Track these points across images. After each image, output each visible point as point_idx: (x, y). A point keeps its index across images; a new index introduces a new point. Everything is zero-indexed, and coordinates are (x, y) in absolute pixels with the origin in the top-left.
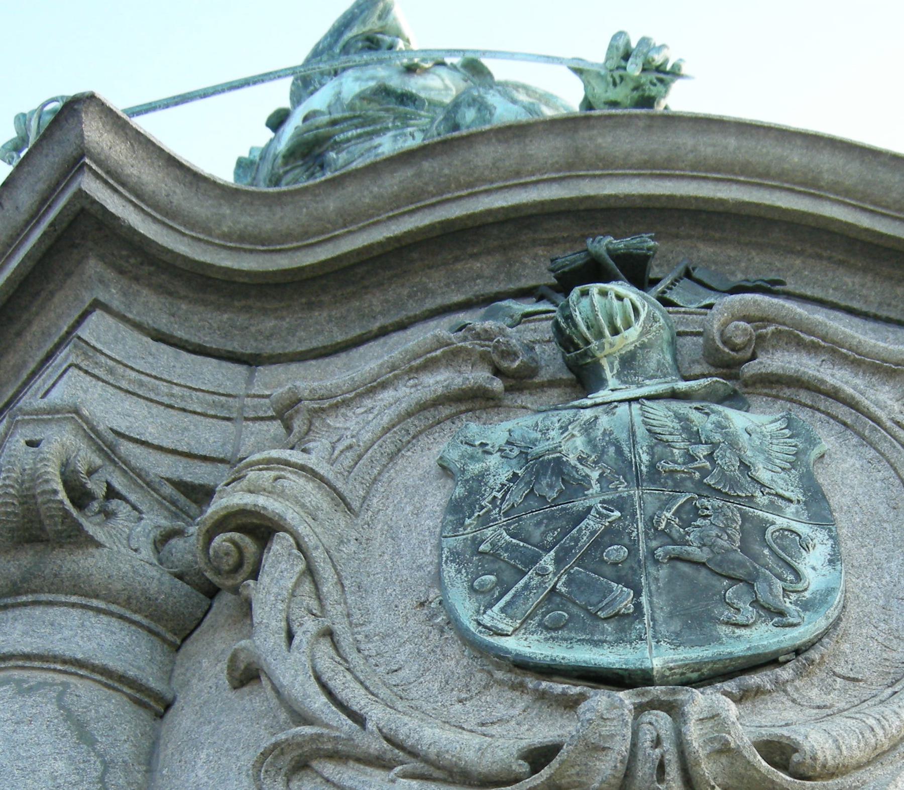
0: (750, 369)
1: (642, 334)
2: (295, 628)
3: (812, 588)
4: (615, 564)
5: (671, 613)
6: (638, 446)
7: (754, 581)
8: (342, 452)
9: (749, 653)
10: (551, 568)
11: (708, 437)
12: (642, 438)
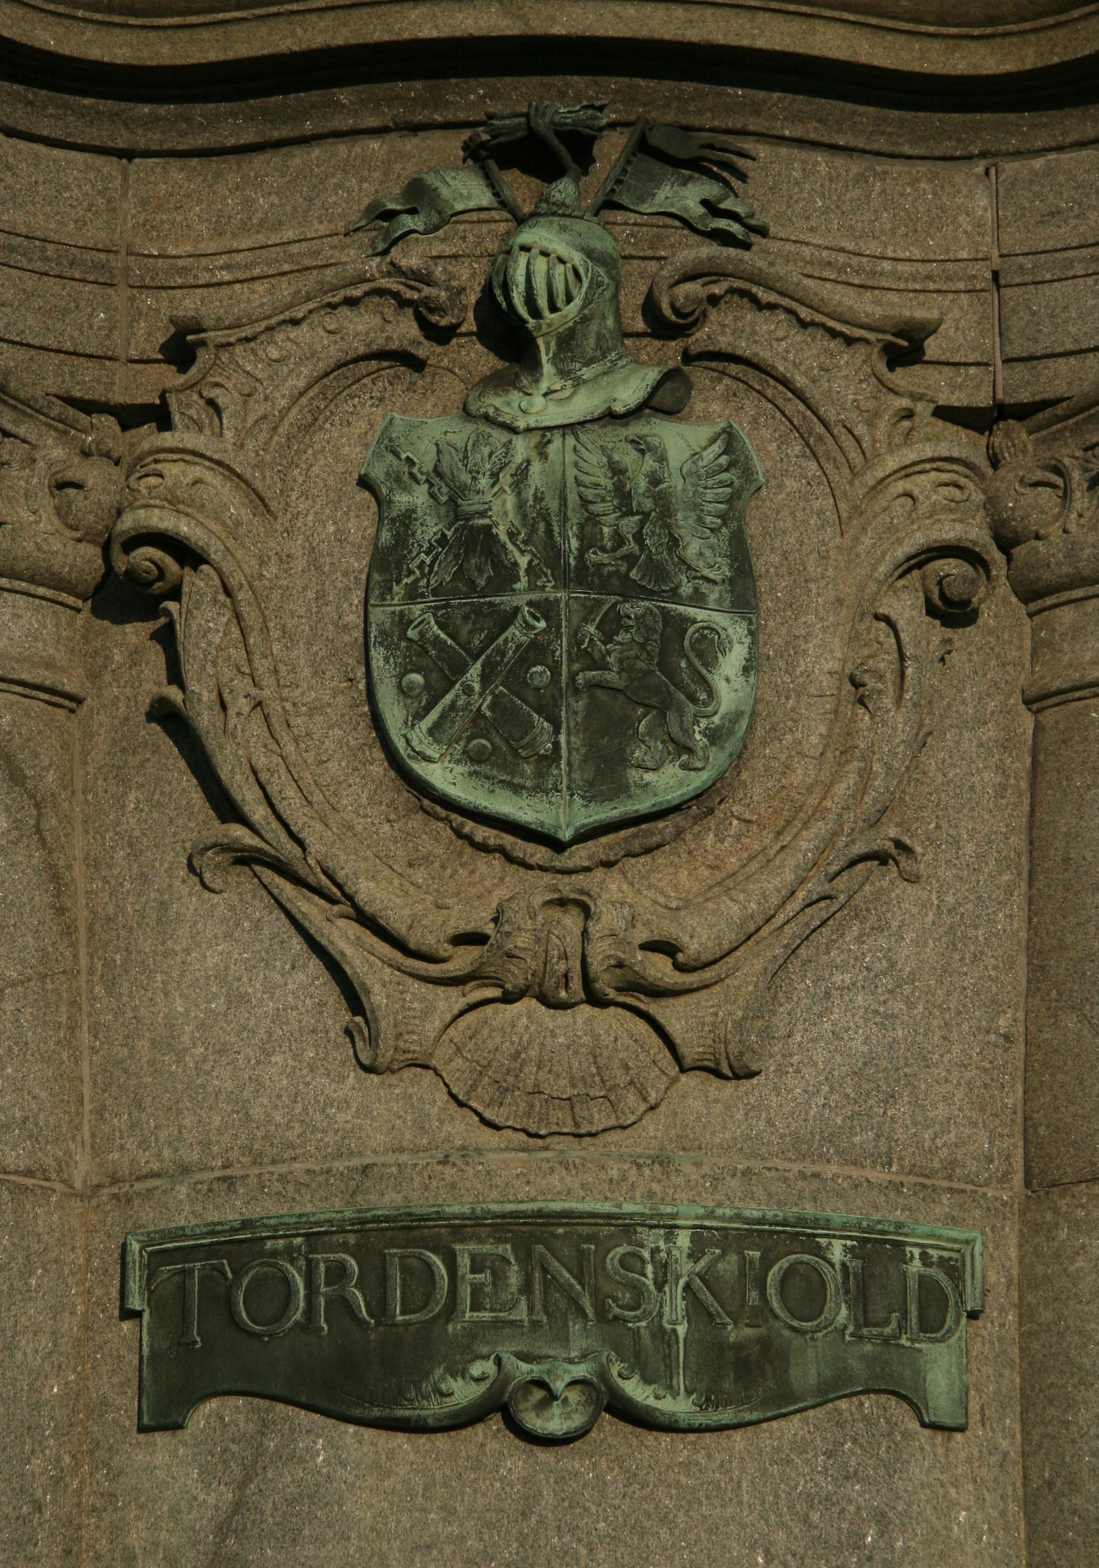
0: (700, 338)
1: (583, 308)
2: (227, 697)
3: (722, 710)
4: (538, 689)
5: (585, 755)
6: (569, 525)
7: (667, 708)
8: (256, 422)
9: (654, 809)
10: (477, 687)
11: (639, 504)
12: (574, 510)
